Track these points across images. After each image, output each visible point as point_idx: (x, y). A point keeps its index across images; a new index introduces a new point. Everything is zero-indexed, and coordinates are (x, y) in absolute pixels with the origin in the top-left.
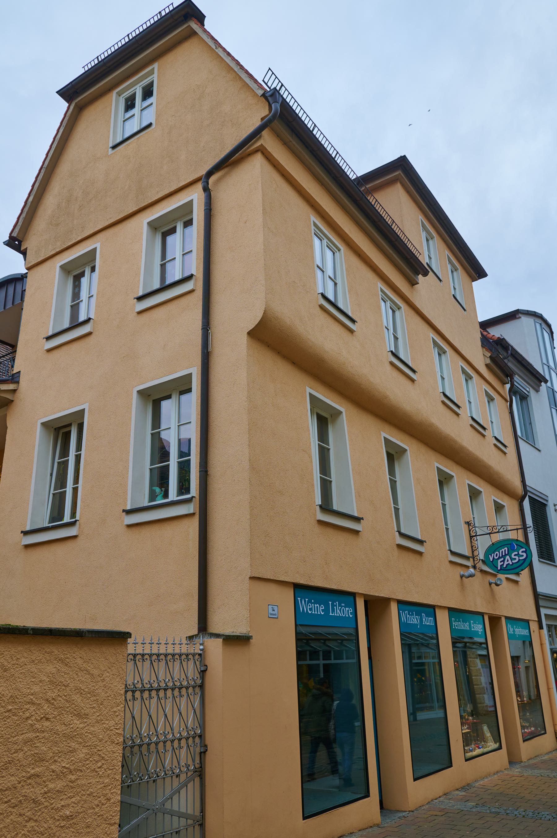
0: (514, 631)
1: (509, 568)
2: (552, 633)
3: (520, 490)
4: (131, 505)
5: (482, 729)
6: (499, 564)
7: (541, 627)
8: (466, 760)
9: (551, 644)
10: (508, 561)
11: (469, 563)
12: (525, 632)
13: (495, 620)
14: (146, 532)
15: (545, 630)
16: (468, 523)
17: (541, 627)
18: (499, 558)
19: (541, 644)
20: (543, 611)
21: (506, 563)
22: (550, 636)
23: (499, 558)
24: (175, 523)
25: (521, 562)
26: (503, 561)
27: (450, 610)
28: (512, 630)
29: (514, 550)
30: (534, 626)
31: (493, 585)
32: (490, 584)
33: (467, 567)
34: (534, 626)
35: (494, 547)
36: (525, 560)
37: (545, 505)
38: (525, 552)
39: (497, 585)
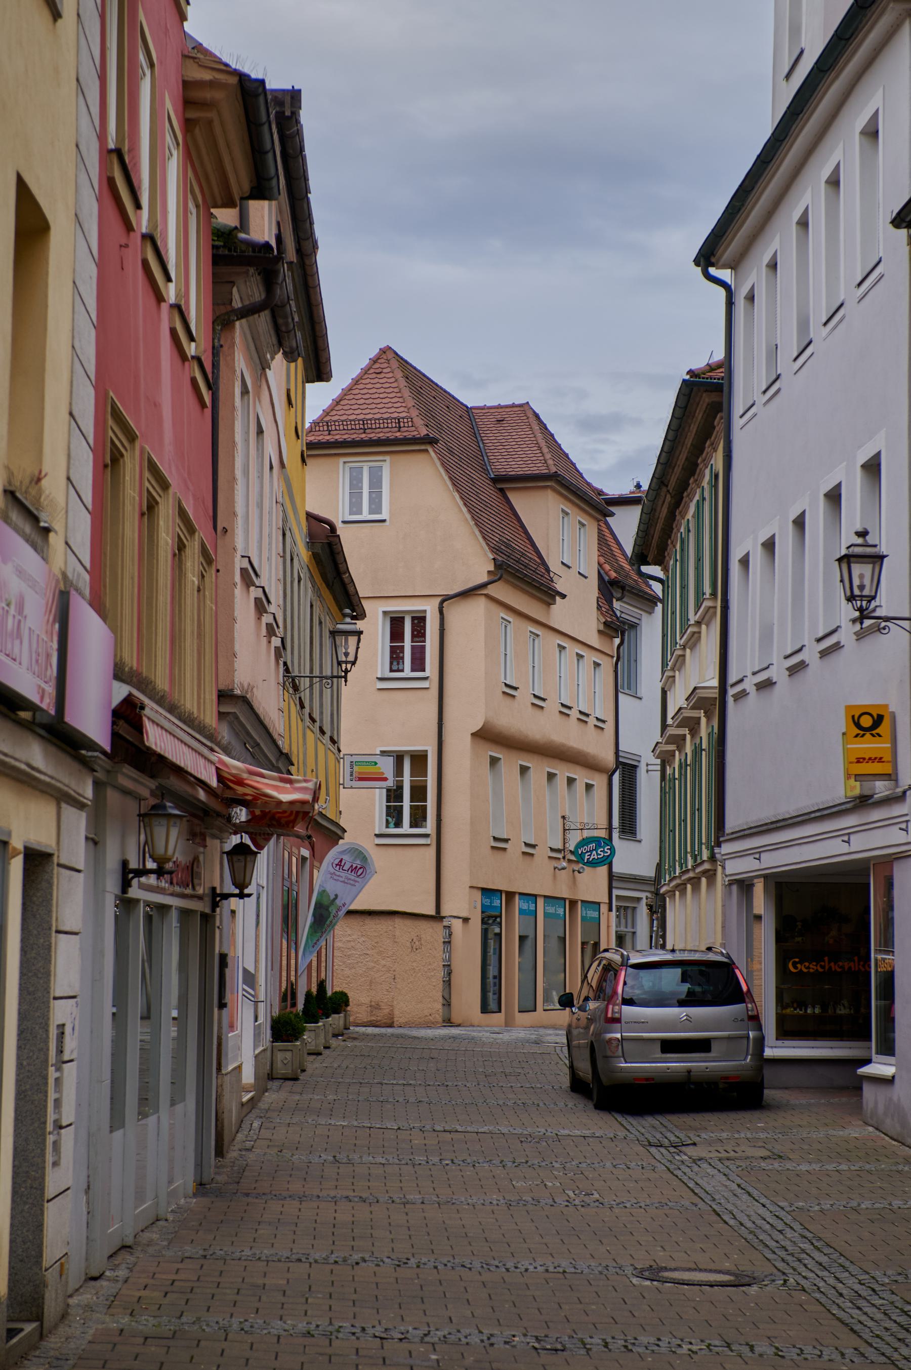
0: (586, 914)
1: (594, 861)
2: (620, 913)
3: (609, 758)
4: (379, 830)
5: (552, 994)
6: (587, 857)
7: (610, 910)
8: (544, 1010)
9: (617, 927)
10: (594, 855)
11: (560, 856)
12: (596, 914)
13: (573, 903)
14: (392, 851)
15: (614, 913)
16: (564, 817)
17: (610, 910)
18: (587, 852)
19: (608, 926)
20: (615, 892)
21: (592, 857)
22: (618, 917)
23: (587, 852)
24: (414, 849)
25: (605, 858)
26: (590, 855)
27: (545, 897)
28: (584, 912)
29: (600, 847)
30: (604, 908)
31: (576, 873)
32: (574, 871)
33: (559, 859)
34: (604, 908)
35: (585, 842)
36: (608, 856)
37: (636, 767)
38: (610, 849)
39: (579, 872)
